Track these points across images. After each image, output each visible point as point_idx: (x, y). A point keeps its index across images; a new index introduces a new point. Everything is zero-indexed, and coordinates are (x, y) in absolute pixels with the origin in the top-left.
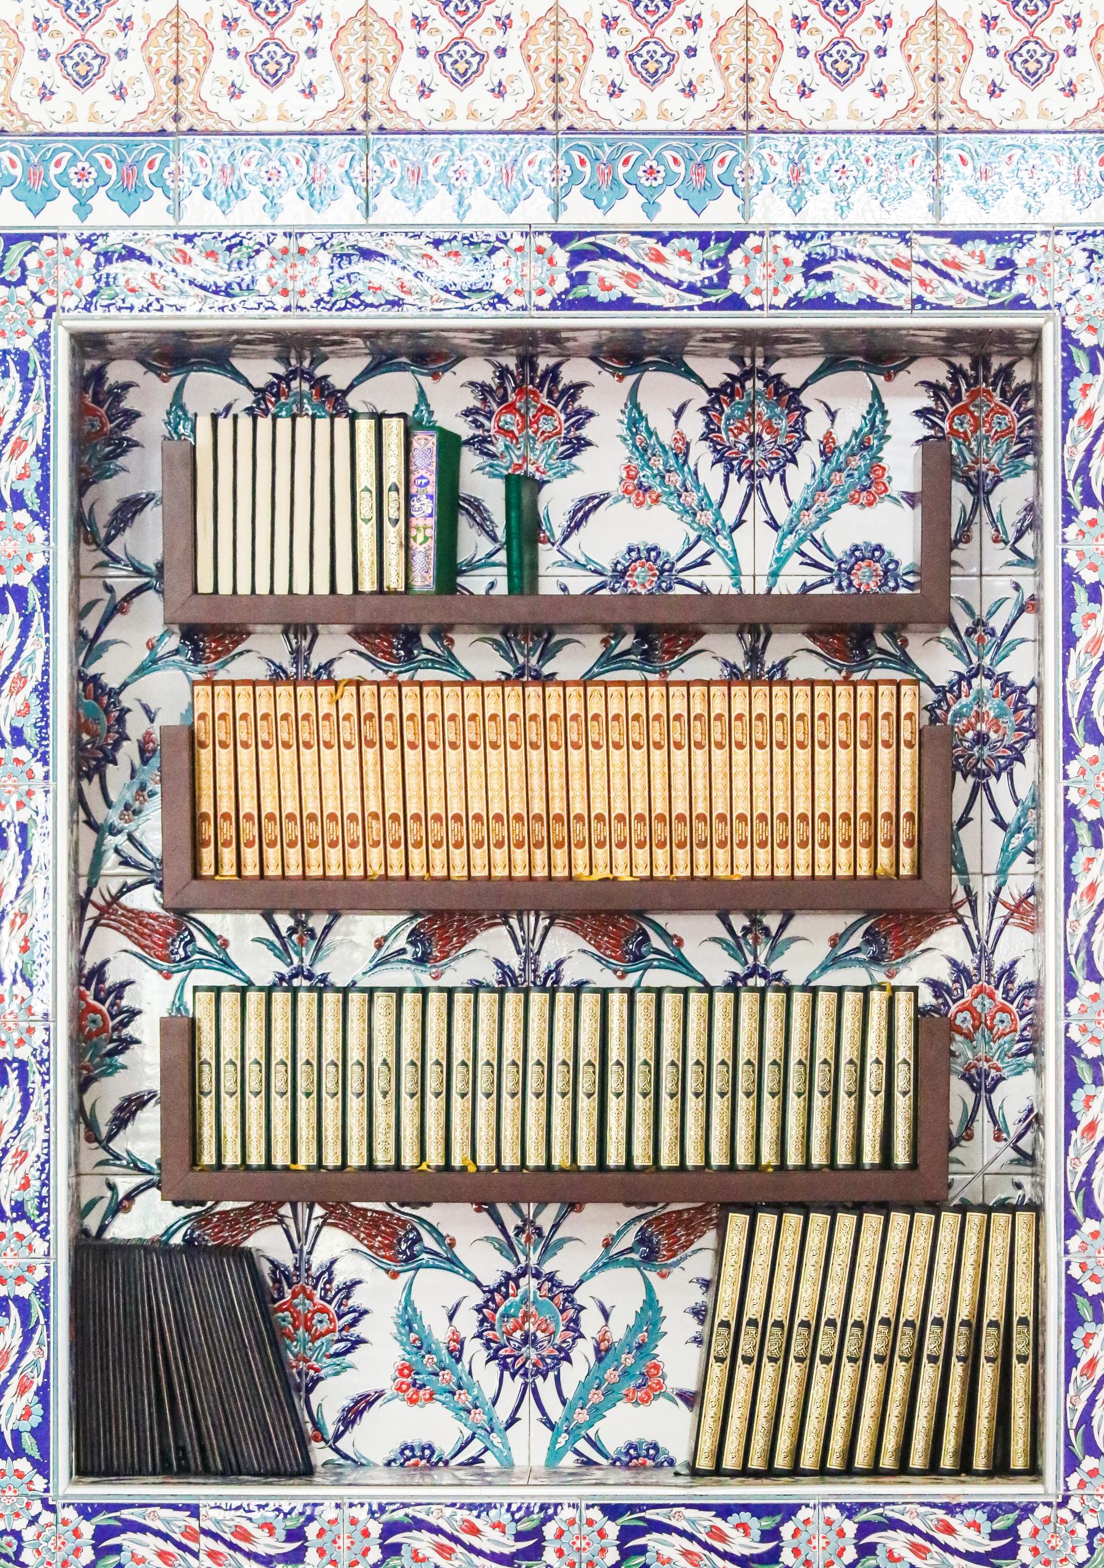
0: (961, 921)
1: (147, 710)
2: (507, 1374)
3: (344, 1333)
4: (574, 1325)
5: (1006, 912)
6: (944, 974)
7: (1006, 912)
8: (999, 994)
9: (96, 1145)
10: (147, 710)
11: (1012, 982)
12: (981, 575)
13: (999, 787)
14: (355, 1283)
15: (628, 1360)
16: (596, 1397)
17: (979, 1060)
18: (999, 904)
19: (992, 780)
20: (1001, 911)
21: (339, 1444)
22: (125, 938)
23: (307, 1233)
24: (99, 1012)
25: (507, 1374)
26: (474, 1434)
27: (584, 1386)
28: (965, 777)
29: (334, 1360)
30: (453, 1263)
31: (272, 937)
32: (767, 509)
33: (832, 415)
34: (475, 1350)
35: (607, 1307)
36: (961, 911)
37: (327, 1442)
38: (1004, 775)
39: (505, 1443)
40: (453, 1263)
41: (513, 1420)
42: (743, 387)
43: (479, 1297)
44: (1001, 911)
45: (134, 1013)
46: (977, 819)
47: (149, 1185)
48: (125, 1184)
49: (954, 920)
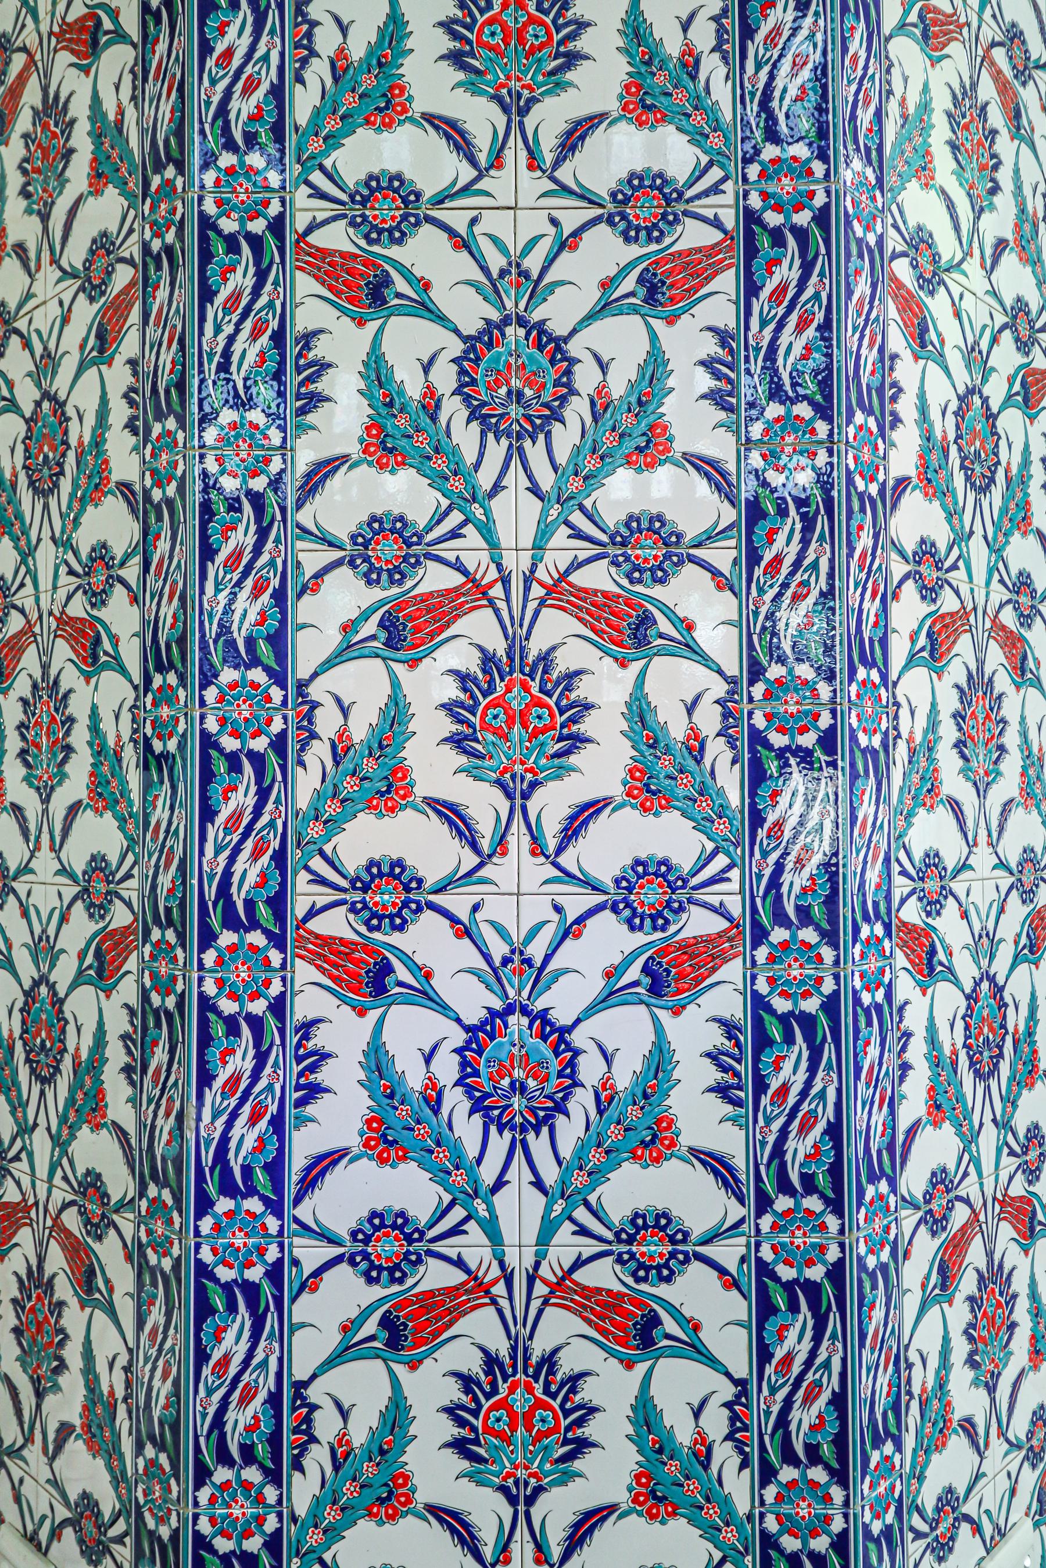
0: (494, 1302)
1: (338, 20)
2: (493, 1129)
3: (565, 731)
4: (570, 1069)
5: (546, 1290)
6: (474, 1365)
7: (546, 1290)
8: (539, 1389)
9: (539, 173)
10: (338, 20)
11: (554, 1374)
12: (518, 894)
13: (539, 1144)
14: (578, 673)
15: (368, 1470)
16: (330, 1516)
17: (516, 1467)
18: (538, 1281)
19: (531, 1136)
20: (540, 1289)
21: (559, 860)
22: (313, 280)
23: (522, 619)
24: (542, 23)
25: (493, 1129)
26: (717, 848)
27: (582, 1146)
28: (500, 1132)
29: (556, 761)
30: (692, 650)
31: (480, 277)
32: (530, 477)
33: (604, 367)
34: (455, 1100)
35: (610, 1050)
36: (494, 1290)
37: (547, 857)
38: (545, 1130)
39: (490, 1208)
40: (692, 650)
41: (500, 1184)
42: (503, 335)
43: (459, 1037)
44: (540, 1289)
45: (582, 25)
46: (719, 898)
47: (337, 564)
48: (570, 221)
49: (487, 1300)
